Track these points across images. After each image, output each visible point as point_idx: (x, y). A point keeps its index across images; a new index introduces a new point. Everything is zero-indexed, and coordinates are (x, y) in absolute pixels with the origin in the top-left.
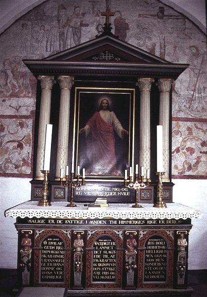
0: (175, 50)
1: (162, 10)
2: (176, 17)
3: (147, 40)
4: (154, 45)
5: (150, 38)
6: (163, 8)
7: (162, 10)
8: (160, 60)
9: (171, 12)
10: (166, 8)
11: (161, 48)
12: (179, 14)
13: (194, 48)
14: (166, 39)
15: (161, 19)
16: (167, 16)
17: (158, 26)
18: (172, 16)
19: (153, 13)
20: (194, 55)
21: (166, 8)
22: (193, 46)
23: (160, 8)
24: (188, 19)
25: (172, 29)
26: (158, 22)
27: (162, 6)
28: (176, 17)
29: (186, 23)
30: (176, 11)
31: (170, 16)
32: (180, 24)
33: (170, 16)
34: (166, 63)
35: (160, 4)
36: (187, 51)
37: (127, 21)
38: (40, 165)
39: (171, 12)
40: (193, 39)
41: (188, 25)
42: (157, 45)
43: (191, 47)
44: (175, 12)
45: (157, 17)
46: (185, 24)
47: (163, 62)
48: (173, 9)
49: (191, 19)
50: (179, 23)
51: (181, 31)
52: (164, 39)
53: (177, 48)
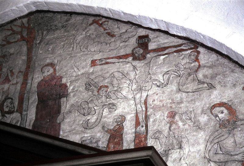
0: (171, 123)
1: (143, 42)
2: (175, 49)
3: (106, 112)
4: (122, 118)
5: (112, 107)
6: (147, 36)
7: (143, 42)
8: (80, 150)
9: (164, 41)
10: (152, 35)
11: (138, 123)
12: (185, 42)
13: (222, 108)
14: (150, 101)
15: (140, 60)
16: (154, 51)
17: (132, 75)
18: (165, 48)
19: (122, 52)
20: (223, 124)
21: (152, 35)
22: (221, 105)
23: (140, 38)
24: (203, 45)
25: (166, 77)
26: (135, 68)
27: (142, 32)
28: (175, 49)
29: (201, 57)
30: (174, 36)
31: (160, 50)
32: (184, 62)
33: (160, 50)
34: (92, 153)
35: (140, 30)
36: (203, 119)
37: (64, 81)
38: (63, 163)
39: (164, 41)
40: (218, 87)
41: (205, 57)
42: (128, 117)
43: (214, 106)
44: (172, 39)
45: (130, 59)
46: (197, 60)
47: (86, 152)
48: (166, 33)
49: (210, 45)
50: (184, 60)
51: (189, 75)
52: (146, 103)
53: (177, 118)
